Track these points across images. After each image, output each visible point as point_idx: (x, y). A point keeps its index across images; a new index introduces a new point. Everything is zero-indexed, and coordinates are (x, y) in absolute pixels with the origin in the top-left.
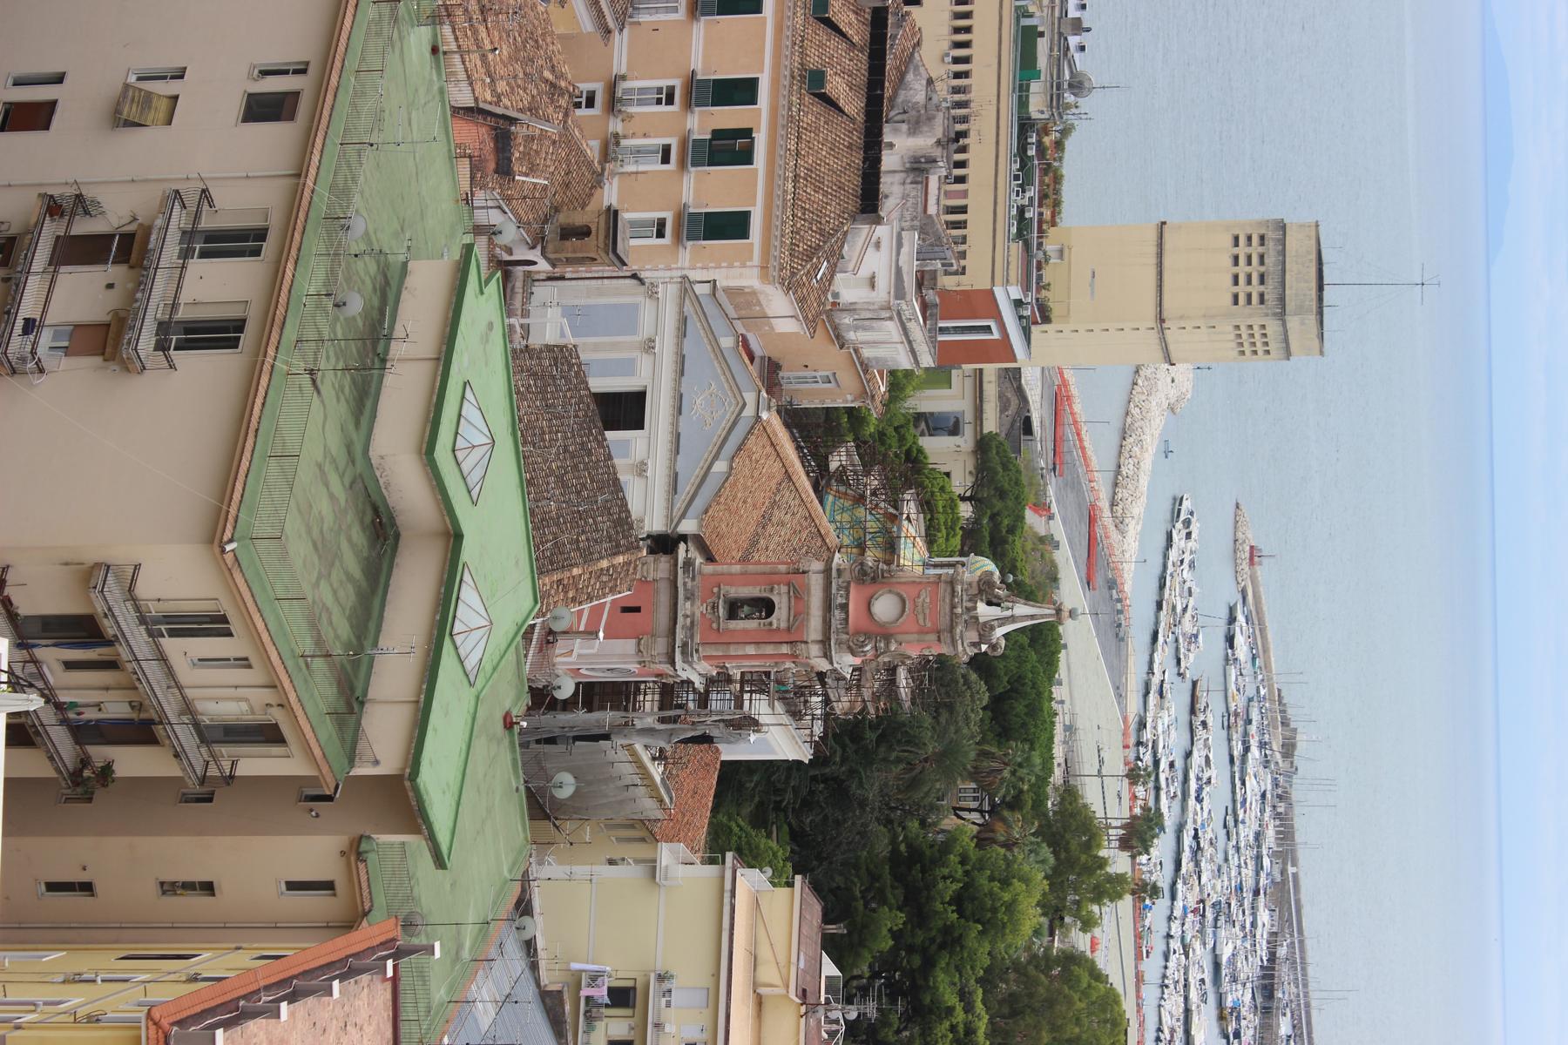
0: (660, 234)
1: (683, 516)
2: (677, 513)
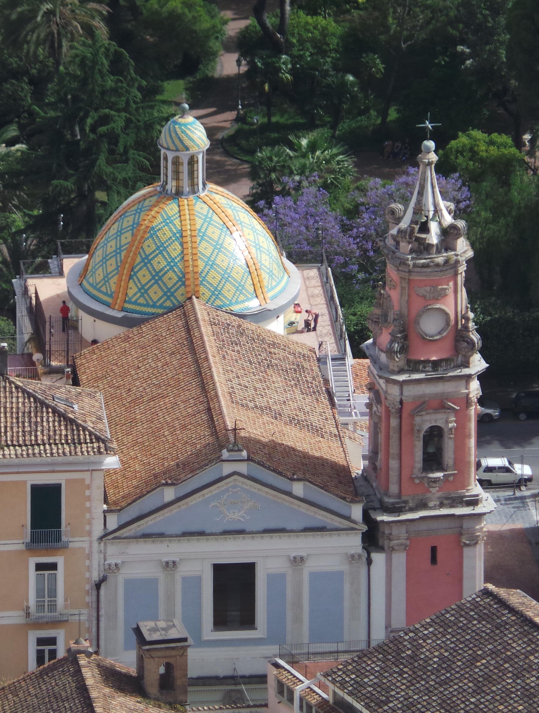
0: (53, 567)
1: (348, 518)
2: (346, 524)
